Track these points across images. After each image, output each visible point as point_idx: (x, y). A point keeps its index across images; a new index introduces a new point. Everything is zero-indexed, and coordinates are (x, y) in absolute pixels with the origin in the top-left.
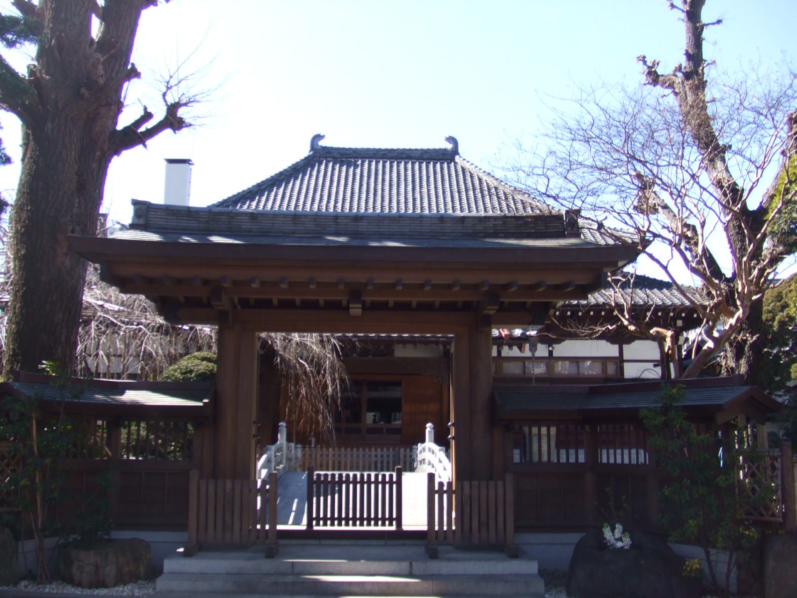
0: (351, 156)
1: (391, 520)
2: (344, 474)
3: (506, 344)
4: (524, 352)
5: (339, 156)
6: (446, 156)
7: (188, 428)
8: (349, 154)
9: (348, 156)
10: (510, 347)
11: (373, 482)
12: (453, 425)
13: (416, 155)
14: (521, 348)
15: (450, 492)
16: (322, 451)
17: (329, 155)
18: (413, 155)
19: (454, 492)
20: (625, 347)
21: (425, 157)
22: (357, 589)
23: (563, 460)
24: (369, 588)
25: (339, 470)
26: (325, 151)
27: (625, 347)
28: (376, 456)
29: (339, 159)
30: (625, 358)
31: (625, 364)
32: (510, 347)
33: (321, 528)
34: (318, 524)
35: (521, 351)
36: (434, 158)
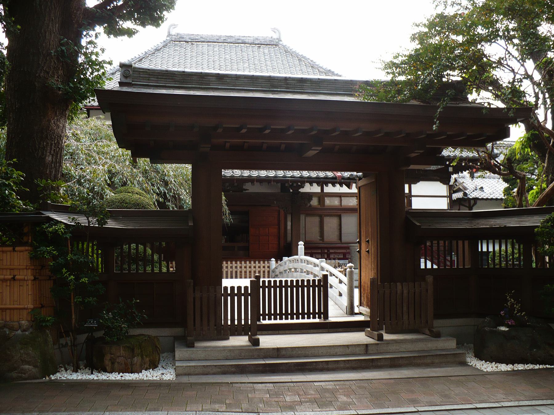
0: (199, 40)
1: (320, 313)
2: (284, 280)
3: (307, 182)
4: (351, 189)
5: (190, 40)
6: (272, 42)
7: (516, 246)
8: (197, 39)
9: (197, 40)
10: (311, 184)
11: (267, 287)
12: (36, 243)
13: (250, 41)
14: (349, 186)
15: (246, 295)
16: (260, 263)
17: (182, 40)
18: (247, 41)
19: (222, 295)
20: (413, 186)
21: (256, 43)
22: (330, 366)
23: (164, 270)
24: (321, 366)
25: (268, 277)
26: (179, 36)
27: (413, 186)
28: (241, 267)
29: (190, 43)
30: (413, 194)
31: (413, 198)
32: (311, 184)
33: (267, 322)
34: (264, 319)
35: (349, 188)
36: (263, 43)
